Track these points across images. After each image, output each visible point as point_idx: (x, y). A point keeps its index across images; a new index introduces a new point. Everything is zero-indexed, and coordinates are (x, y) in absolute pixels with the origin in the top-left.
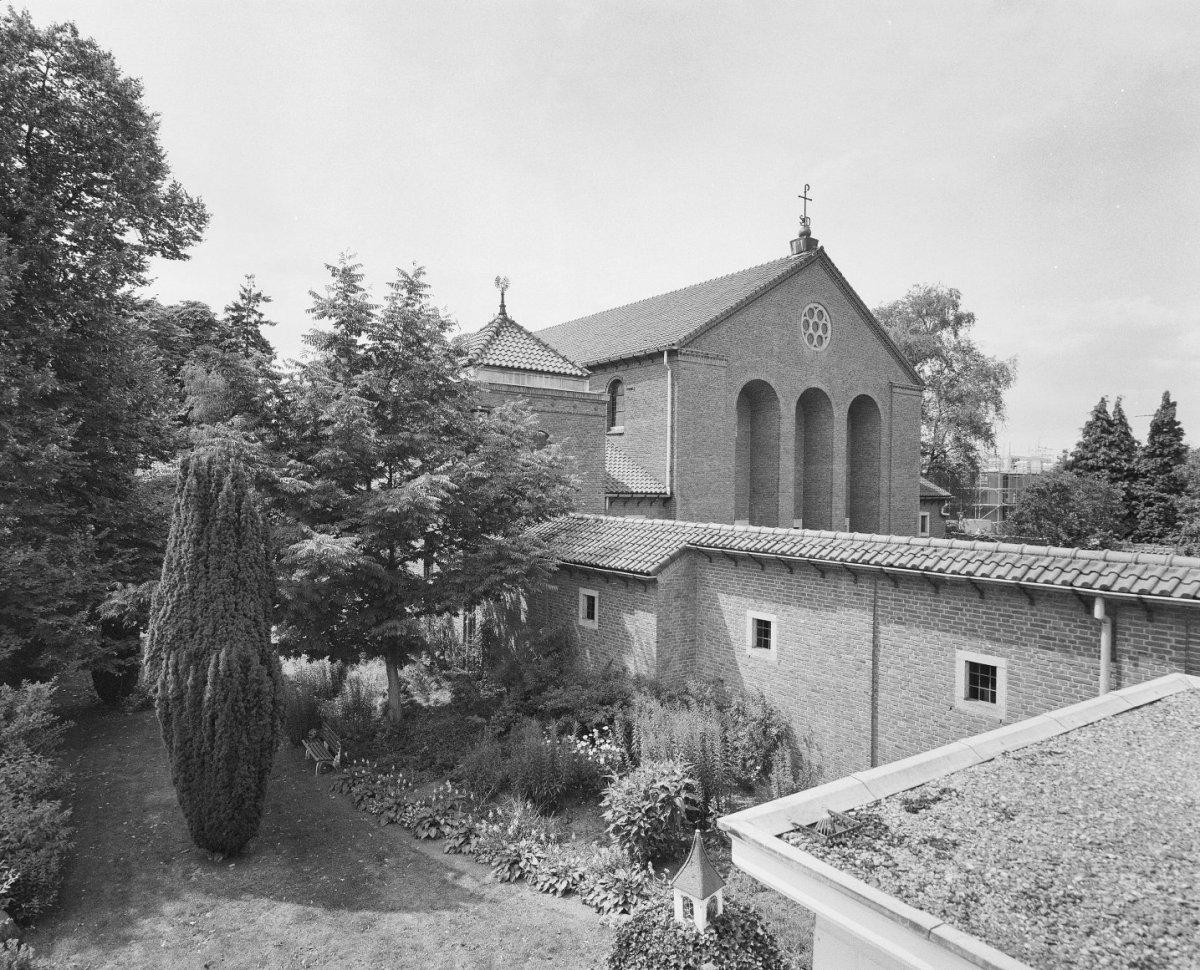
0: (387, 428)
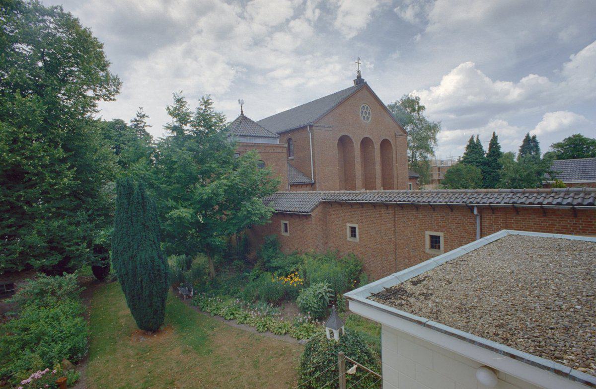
0: (201, 161)
